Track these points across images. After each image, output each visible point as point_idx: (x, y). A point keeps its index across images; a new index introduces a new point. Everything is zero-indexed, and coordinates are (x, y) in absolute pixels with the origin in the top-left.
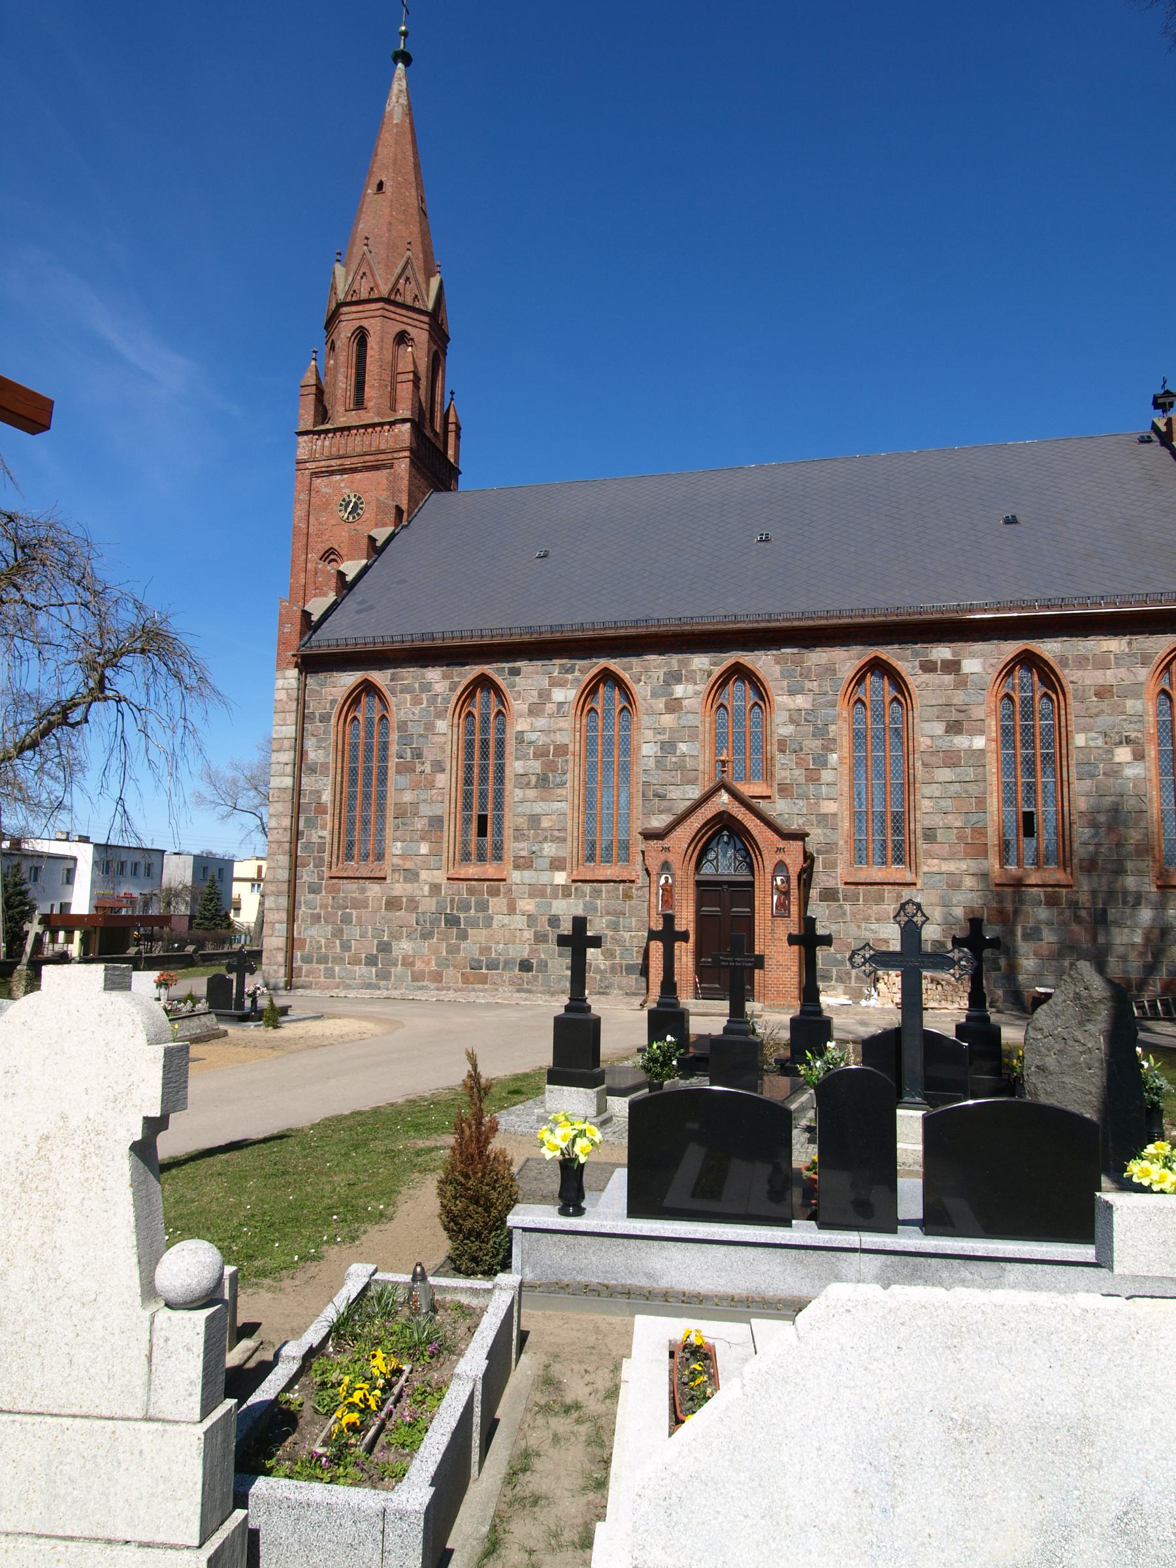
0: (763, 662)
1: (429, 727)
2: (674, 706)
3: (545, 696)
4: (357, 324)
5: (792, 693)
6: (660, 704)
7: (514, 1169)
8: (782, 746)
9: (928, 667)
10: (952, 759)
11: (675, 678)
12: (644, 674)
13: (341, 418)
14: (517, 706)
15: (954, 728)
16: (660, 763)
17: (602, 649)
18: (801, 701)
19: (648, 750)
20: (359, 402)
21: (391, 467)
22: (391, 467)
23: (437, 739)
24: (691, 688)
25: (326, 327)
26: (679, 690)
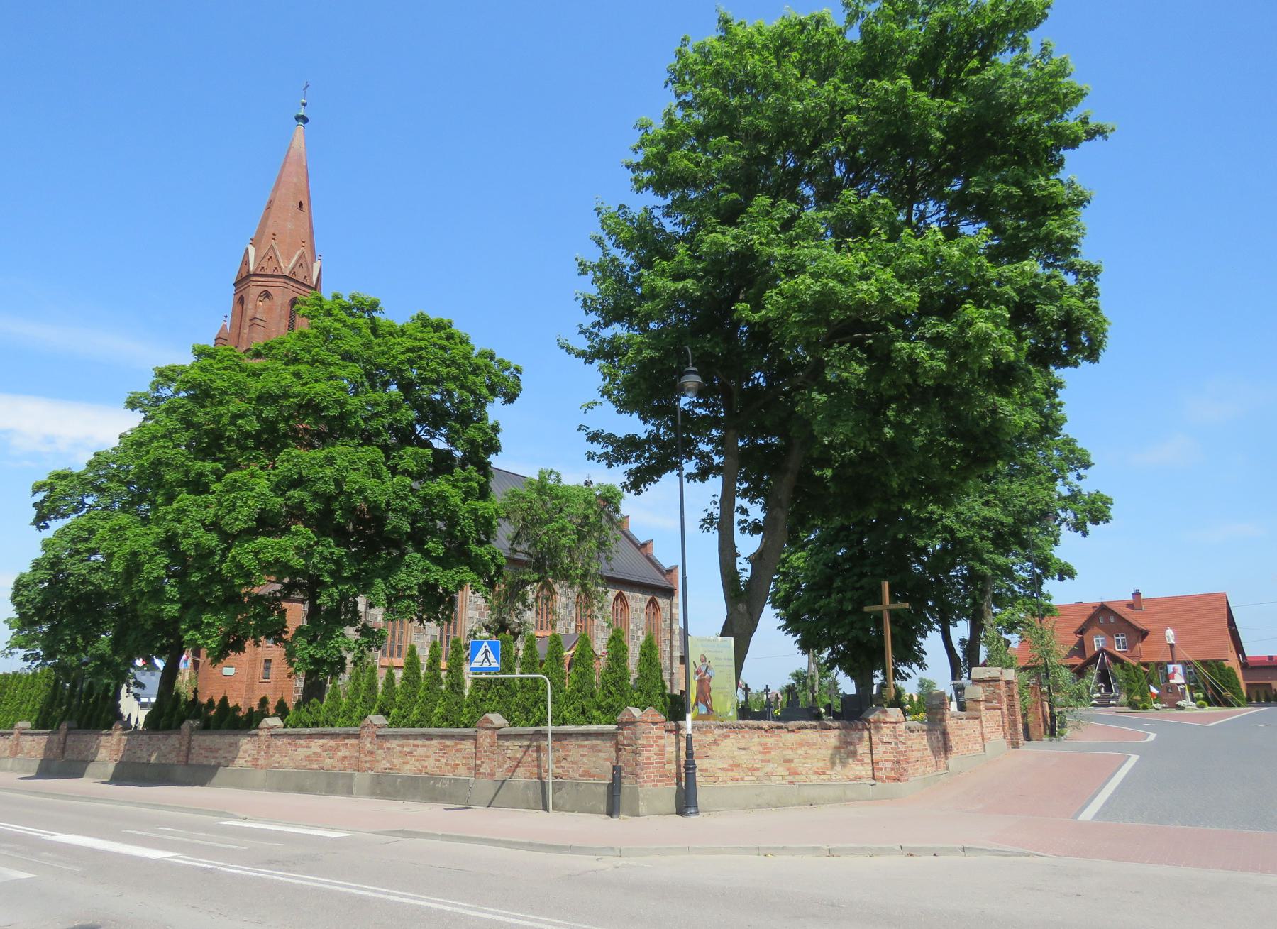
4: (295, 295)
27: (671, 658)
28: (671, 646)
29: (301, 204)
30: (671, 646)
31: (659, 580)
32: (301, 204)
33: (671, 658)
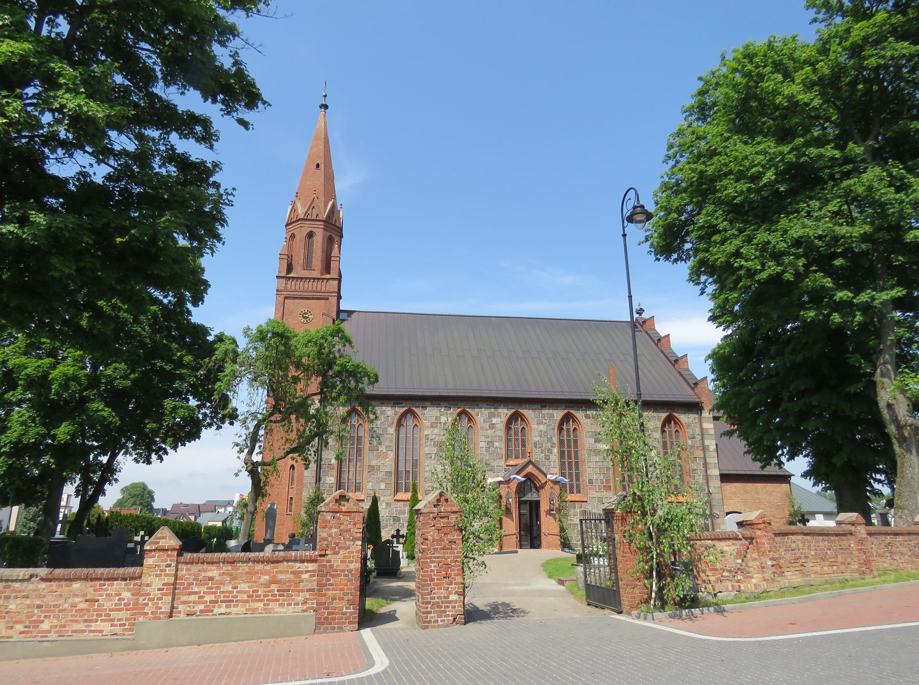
0: (528, 413)
1: (385, 430)
2: (492, 426)
3: (438, 418)
4: (310, 230)
5: (538, 424)
6: (487, 425)
7: (211, 338)
8: (535, 445)
9: (587, 417)
10: (597, 452)
11: (492, 415)
12: (480, 415)
13: (298, 272)
14: (426, 423)
15: (597, 441)
16: (487, 449)
17: (463, 403)
18: (542, 427)
19: (483, 445)
20: (308, 265)
21: (328, 299)
22: (328, 299)
23: (388, 436)
24: (499, 420)
25: (333, 229)
26: (494, 420)
27: (707, 477)
28: (705, 465)
29: (318, 166)
30: (705, 465)
31: (688, 396)
32: (318, 166)
33: (707, 477)
